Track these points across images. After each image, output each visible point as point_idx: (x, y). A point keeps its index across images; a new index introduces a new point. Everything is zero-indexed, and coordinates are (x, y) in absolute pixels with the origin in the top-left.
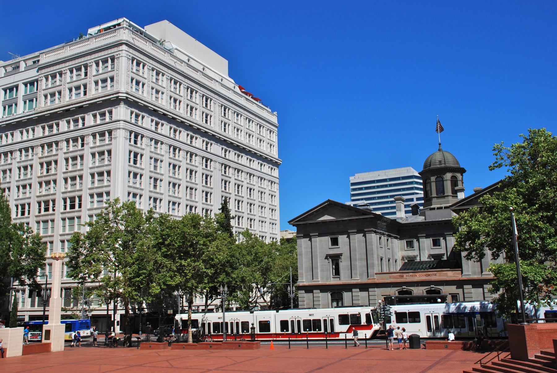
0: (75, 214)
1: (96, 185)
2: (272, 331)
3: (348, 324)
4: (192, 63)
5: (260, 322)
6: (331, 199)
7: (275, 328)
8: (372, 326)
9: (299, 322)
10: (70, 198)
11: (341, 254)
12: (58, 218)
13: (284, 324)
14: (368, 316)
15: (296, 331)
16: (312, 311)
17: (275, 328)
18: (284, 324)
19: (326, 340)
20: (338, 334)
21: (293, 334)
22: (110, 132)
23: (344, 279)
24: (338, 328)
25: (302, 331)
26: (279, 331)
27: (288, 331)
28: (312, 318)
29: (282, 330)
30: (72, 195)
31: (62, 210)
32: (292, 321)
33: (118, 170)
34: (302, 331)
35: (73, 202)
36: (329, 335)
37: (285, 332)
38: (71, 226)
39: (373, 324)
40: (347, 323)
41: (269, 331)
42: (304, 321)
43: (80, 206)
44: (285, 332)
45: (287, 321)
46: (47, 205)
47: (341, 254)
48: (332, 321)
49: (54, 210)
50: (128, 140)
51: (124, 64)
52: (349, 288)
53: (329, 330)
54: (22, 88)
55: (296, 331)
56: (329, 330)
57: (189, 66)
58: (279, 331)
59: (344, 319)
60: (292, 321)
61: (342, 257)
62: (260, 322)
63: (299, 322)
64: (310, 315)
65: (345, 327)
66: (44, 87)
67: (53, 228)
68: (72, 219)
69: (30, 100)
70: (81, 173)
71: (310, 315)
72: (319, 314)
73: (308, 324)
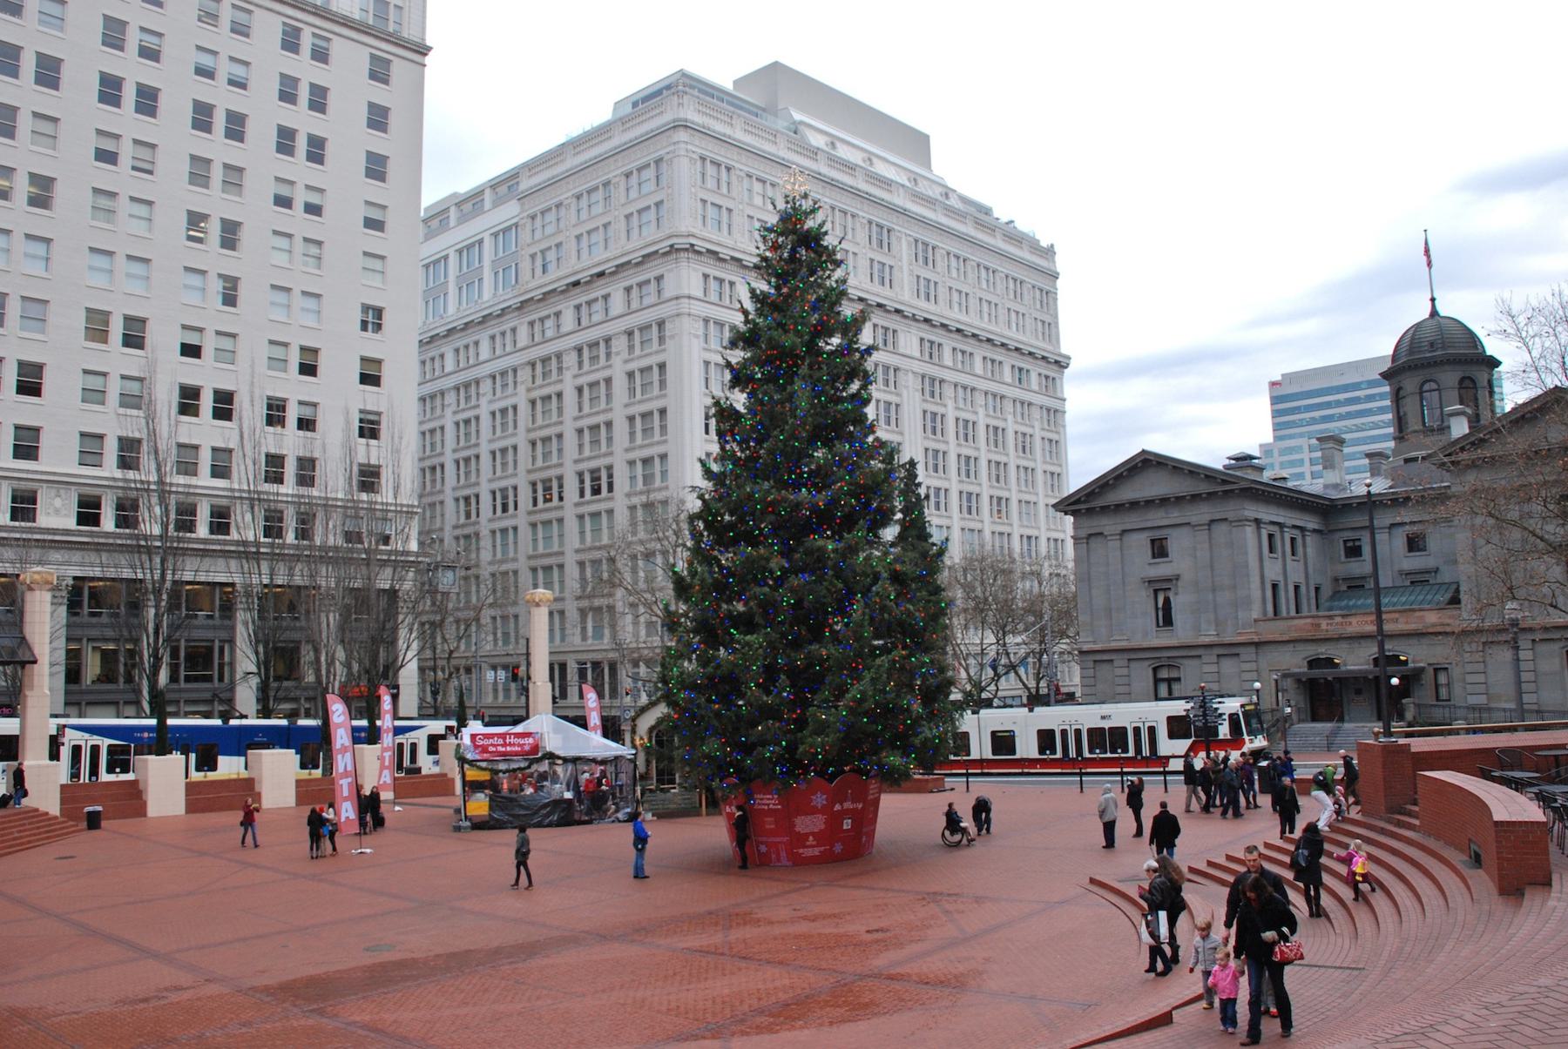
0: (602, 506)
1: (587, 453)
2: (975, 754)
3: (1188, 737)
4: (843, 152)
5: (993, 733)
6: (1148, 448)
7: (1027, 747)
8: (1243, 742)
9: (1078, 732)
10: (544, 481)
11: (1177, 578)
12: (569, 513)
13: (1046, 739)
14: (1234, 719)
15: (1072, 753)
16: (1106, 709)
17: (1027, 747)
18: (1046, 739)
19: (1081, 774)
20: (1166, 760)
21: (1065, 761)
22: (661, 324)
23: (1182, 632)
24: (1167, 746)
25: (1087, 754)
26: (988, 754)
27: (1054, 752)
28: (1106, 725)
29: (1041, 751)
30: (593, 464)
31: (576, 498)
32: (1064, 732)
33: (190, 486)
34: (1087, 754)
35: (597, 483)
36: (1146, 761)
37: (1048, 756)
38: (597, 531)
39: (1246, 737)
40: (1186, 736)
41: (968, 754)
42: (1090, 730)
43: (611, 489)
44: (1048, 756)
45: (1052, 732)
46: (548, 490)
47: (1177, 578)
48: (1152, 730)
49: (561, 499)
50: (702, 339)
51: (684, 172)
52: (1192, 650)
53: (1146, 751)
54: (453, 260)
55: (1072, 753)
56: (1146, 751)
57: (834, 161)
58: (988, 754)
59: (1178, 727)
60: (1064, 732)
61: (1180, 583)
62: (993, 733)
63: (1078, 732)
64: (1103, 718)
65: (1182, 745)
66: (529, 240)
67: (561, 536)
68: (596, 515)
69: (503, 268)
70: (608, 416)
71: (1103, 718)
72: (1124, 714)
73: (1097, 736)
